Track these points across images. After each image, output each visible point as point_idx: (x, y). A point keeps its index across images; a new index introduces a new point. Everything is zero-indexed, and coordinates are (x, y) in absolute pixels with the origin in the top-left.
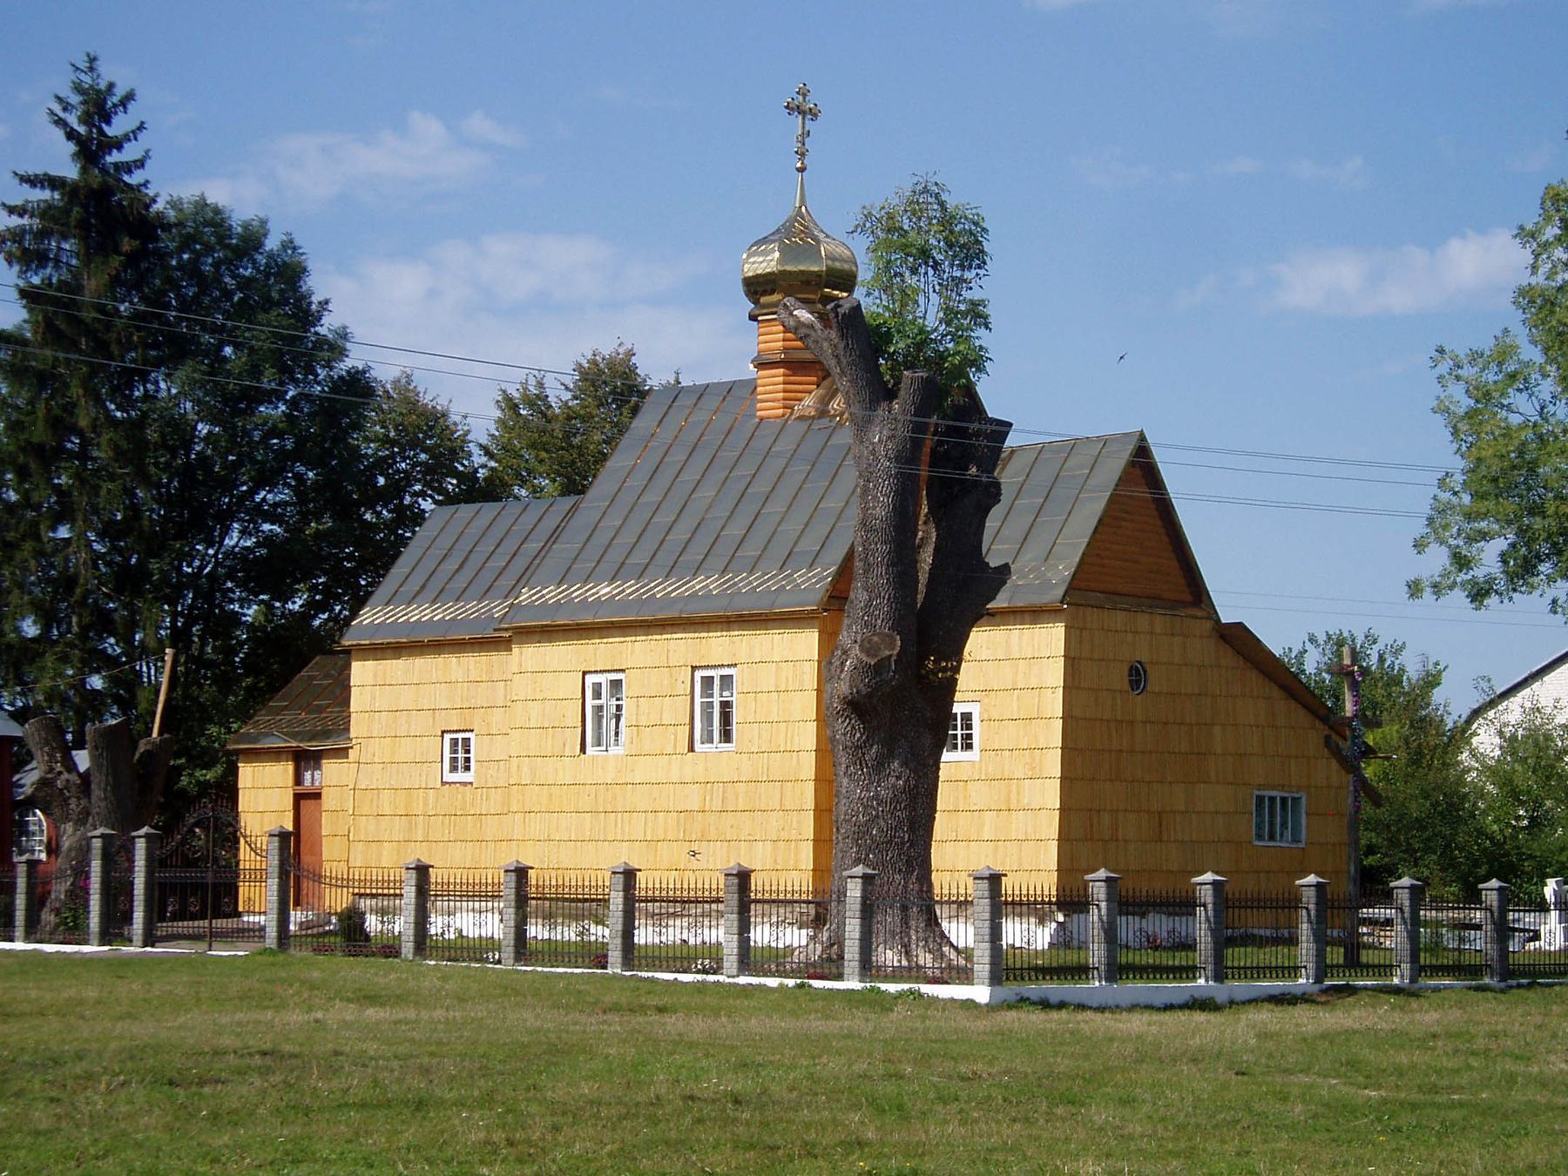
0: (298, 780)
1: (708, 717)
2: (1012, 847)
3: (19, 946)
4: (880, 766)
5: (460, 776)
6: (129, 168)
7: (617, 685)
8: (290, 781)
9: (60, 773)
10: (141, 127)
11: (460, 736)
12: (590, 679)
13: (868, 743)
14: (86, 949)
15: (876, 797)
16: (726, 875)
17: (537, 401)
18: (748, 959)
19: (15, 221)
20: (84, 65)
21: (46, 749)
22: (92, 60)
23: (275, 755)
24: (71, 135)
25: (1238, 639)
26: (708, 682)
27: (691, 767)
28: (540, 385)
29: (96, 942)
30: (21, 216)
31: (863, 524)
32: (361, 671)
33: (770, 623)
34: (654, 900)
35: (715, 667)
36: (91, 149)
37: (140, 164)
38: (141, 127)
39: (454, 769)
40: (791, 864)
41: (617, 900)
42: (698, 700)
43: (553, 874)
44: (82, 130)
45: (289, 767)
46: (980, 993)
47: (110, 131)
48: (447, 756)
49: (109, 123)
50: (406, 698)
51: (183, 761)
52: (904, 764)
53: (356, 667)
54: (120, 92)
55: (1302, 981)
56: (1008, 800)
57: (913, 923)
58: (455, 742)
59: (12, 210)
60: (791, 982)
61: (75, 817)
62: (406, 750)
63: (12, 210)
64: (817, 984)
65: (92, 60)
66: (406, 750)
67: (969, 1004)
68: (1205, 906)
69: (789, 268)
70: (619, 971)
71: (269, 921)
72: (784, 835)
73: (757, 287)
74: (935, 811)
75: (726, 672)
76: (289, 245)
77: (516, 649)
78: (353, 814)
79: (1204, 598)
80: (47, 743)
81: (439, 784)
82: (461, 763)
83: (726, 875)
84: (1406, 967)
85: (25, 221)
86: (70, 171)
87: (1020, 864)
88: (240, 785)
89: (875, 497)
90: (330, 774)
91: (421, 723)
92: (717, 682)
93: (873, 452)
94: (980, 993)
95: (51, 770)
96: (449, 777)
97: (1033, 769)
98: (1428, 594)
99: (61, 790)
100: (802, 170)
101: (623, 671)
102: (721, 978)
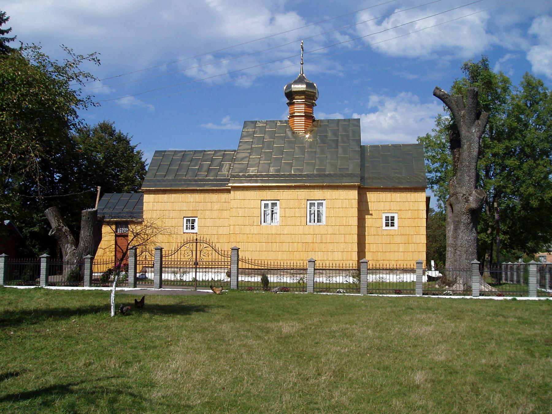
2: (411, 254)
3: (87, 288)
6: (8, 40)
9: (63, 227)
11: (191, 219)
16: (417, 263)
18: (162, 283)
21: (56, 218)
29: (133, 287)
32: (147, 198)
33: (339, 188)
34: (293, 269)
35: (315, 200)
39: (187, 229)
40: (349, 258)
43: (301, 262)
45: (114, 227)
48: (185, 224)
50: (169, 206)
51: (24, 225)
54: (7, 16)
56: (408, 241)
61: (70, 242)
64: (518, 298)
70: (421, 295)
72: (345, 250)
74: (426, 244)
78: (197, 242)
81: (182, 233)
83: (417, 263)
87: (413, 258)
92: (316, 205)
95: (59, 225)
96: (185, 231)
97: (417, 232)
99: (64, 233)
101: (278, 200)
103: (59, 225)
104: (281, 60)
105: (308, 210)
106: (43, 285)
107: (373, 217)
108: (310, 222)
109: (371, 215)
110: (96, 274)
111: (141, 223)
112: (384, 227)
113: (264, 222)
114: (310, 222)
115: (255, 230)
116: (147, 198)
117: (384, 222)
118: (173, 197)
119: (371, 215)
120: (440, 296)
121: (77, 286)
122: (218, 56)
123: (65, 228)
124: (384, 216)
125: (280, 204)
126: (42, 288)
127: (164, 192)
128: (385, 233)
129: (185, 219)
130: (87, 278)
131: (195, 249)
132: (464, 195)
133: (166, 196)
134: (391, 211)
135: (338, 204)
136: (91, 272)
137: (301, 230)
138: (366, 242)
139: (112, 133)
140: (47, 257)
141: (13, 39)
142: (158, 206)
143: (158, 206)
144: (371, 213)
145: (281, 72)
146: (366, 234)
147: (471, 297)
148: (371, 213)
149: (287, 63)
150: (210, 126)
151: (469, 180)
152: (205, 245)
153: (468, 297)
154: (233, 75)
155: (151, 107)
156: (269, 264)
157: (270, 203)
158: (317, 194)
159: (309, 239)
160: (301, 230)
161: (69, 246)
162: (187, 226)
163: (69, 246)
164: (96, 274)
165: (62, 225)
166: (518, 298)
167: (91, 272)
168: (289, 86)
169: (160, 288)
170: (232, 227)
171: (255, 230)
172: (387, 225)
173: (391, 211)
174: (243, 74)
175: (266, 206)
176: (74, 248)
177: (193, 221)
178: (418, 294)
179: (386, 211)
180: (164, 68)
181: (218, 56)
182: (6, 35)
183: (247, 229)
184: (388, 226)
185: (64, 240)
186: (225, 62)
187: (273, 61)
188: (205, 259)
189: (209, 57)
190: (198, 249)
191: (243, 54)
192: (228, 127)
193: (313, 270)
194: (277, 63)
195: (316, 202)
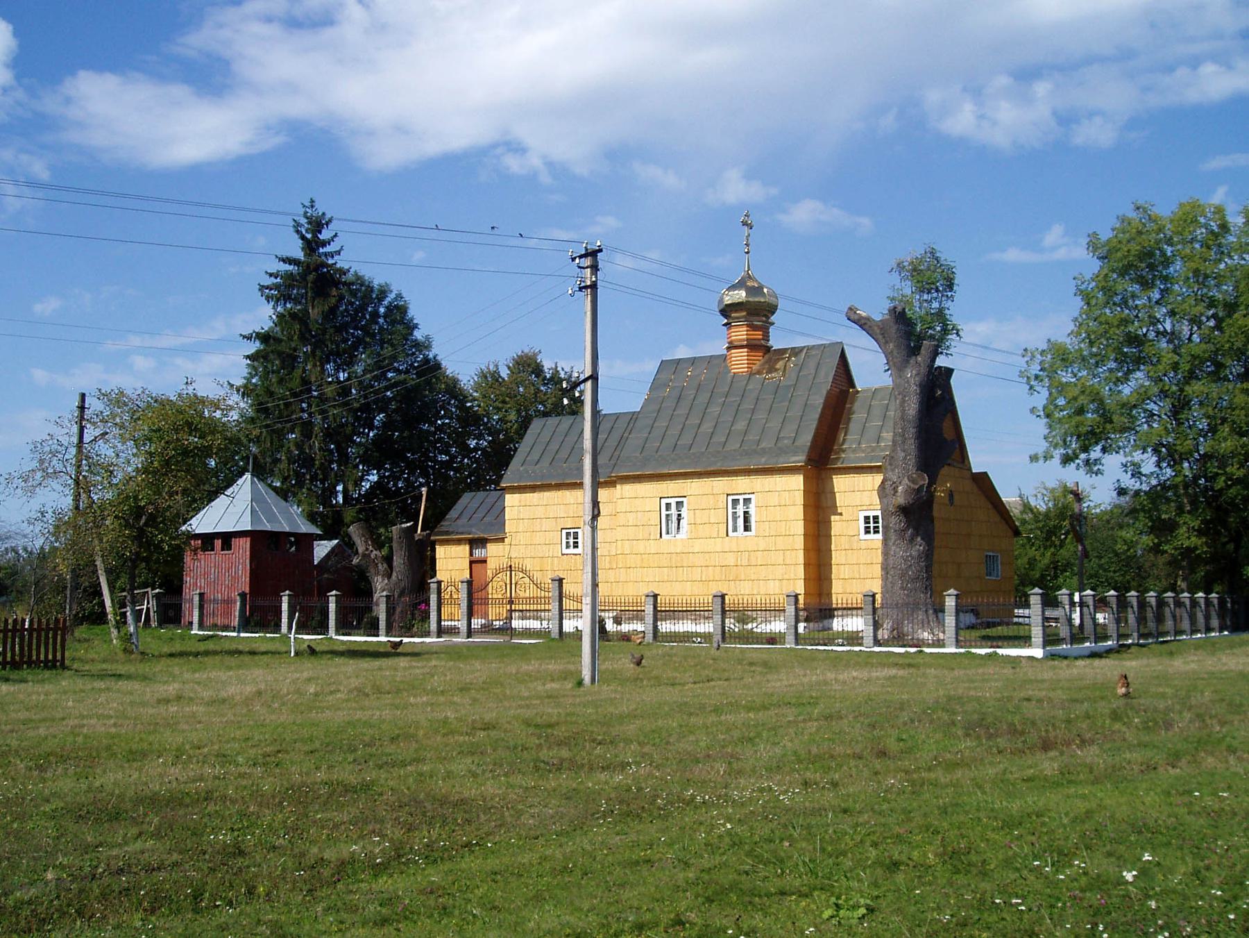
0: (471, 554)
1: (735, 518)
3: (383, 639)
4: (912, 540)
5: (572, 550)
7: (679, 504)
8: (468, 555)
10: (336, 235)
11: (572, 531)
12: (664, 501)
13: (908, 528)
14: (427, 640)
15: (911, 555)
17: (496, 376)
19: (273, 280)
20: (308, 204)
22: (312, 201)
23: (459, 542)
24: (303, 238)
25: (983, 481)
26: (735, 502)
27: (728, 544)
28: (497, 366)
29: (435, 635)
30: (276, 278)
31: (902, 418)
32: (510, 499)
36: (312, 245)
37: (338, 253)
38: (336, 235)
39: (568, 547)
41: (649, 609)
42: (730, 511)
43: (680, 598)
44: (309, 236)
45: (467, 547)
46: (1038, 653)
47: (321, 237)
48: (564, 541)
49: (320, 233)
50: (540, 512)
52: (922, 539)
53: (508, 497)
54: (328, 216)
55: (1110, 643)
57: (930, 618)
58: (568, 534)
59: (271, 275)
60: (913, 650)
62: (539, 538)
63: (271, 275)
65: (312, 201)
66: (539, 538)
67: (1031, 658)
68: (1088, 606)
69: (751, 299)
71: (462, 625)
72: (786, 577)
73: (726, 311)
75: (747, 496)
76: (399, 296)
77: (618, 487)
79: (966, 461)
80: (363, 536)
82: (572, 544)
84: (1135, 635)
85: (278, 280)
86: (300, 254)
88: (437, 556)
89: (909, 405)
90: (494, 553)
91: (548, 524)
92: (741, 502)
93: (908, 382)
94: (1038, 653)
95: (367, 549)
96: (565, 551)
98: (1041, 461)
100: (748, 253)
102: (863, 649)
103: (367, 549)
104: (1195, 62)
105: (730, 511)
106: (332, 633)
107: (843, 518)
108: (735, 530)
109: (841, 514)
110: (446, 623)
111: (502, 540)
112: (863, 536)
113: (668, 533)
114: (735, 530)
115: (653, 546)
116: (510, 499)
117: (862, 525)
118: (547, 495)
119: (841, 514)
120: (830, 648)
121: (349, 634)
122: (1026, 75)
123: (375, 552)
124: (862, 515)
125: (688, 504)
126: (331, 638)
127: (533, 488)
128: (863, 545)
129: (564, 532)
130: (433, 626)
131: (508, 582)
132: (894, 483)
133: (536, 495)
134: (872, 507)
135: (773, 499)
136: (439, 620)
137: (718, 545)
138: (833, 562)
139: (538, 370)
140: (336, 595)
141: (338, 253)
142: (525, 513)
143: (525, 513)
144: (839, 511)
145: (1192, 96)
146: (833, 547)
147: (863, 649)
148: (839, 511)
149: (1209, 69)
150: (1013, 255)
151: (905, 458)
152: (521, 575)
153: (857, 649)
154: (1066, 119)
155: (865, 221)
156: (773, 601)
157: (673, 501)
158: (742, 484)
159: (730, 559)
160: (718, 545)
161: (380, 580)
162: (567, 543)
163: (380, 578)
164: (446, 623)
165: (371, 548)
166: (973, 650)
167: (439, 620)
168: (721, 300)
169: (468, 637)
170: (619, 543)
171: (653, 546)
172: (867, 531)
173: (872, 507)
174: (1091, 114)
175: (668, 506)
176: (386, 581)
177: (576, 536)
178: (789, 643)
179: (865, 508)
180: (888, 122)
181: (1026, 75)
182: (328, 249)
183: (640, 546)
184: (869, 532)
185: (372, 571)
186: (1042, 89)
187: (1170, 69)
188: (522, 594)
189: (1003, 81)
190: (513, 582)
191: (1091, 60)
192: (1061, 254)
193: (1040, 621)
194: (1182, 73)
195: (741, 498)
